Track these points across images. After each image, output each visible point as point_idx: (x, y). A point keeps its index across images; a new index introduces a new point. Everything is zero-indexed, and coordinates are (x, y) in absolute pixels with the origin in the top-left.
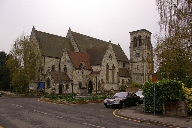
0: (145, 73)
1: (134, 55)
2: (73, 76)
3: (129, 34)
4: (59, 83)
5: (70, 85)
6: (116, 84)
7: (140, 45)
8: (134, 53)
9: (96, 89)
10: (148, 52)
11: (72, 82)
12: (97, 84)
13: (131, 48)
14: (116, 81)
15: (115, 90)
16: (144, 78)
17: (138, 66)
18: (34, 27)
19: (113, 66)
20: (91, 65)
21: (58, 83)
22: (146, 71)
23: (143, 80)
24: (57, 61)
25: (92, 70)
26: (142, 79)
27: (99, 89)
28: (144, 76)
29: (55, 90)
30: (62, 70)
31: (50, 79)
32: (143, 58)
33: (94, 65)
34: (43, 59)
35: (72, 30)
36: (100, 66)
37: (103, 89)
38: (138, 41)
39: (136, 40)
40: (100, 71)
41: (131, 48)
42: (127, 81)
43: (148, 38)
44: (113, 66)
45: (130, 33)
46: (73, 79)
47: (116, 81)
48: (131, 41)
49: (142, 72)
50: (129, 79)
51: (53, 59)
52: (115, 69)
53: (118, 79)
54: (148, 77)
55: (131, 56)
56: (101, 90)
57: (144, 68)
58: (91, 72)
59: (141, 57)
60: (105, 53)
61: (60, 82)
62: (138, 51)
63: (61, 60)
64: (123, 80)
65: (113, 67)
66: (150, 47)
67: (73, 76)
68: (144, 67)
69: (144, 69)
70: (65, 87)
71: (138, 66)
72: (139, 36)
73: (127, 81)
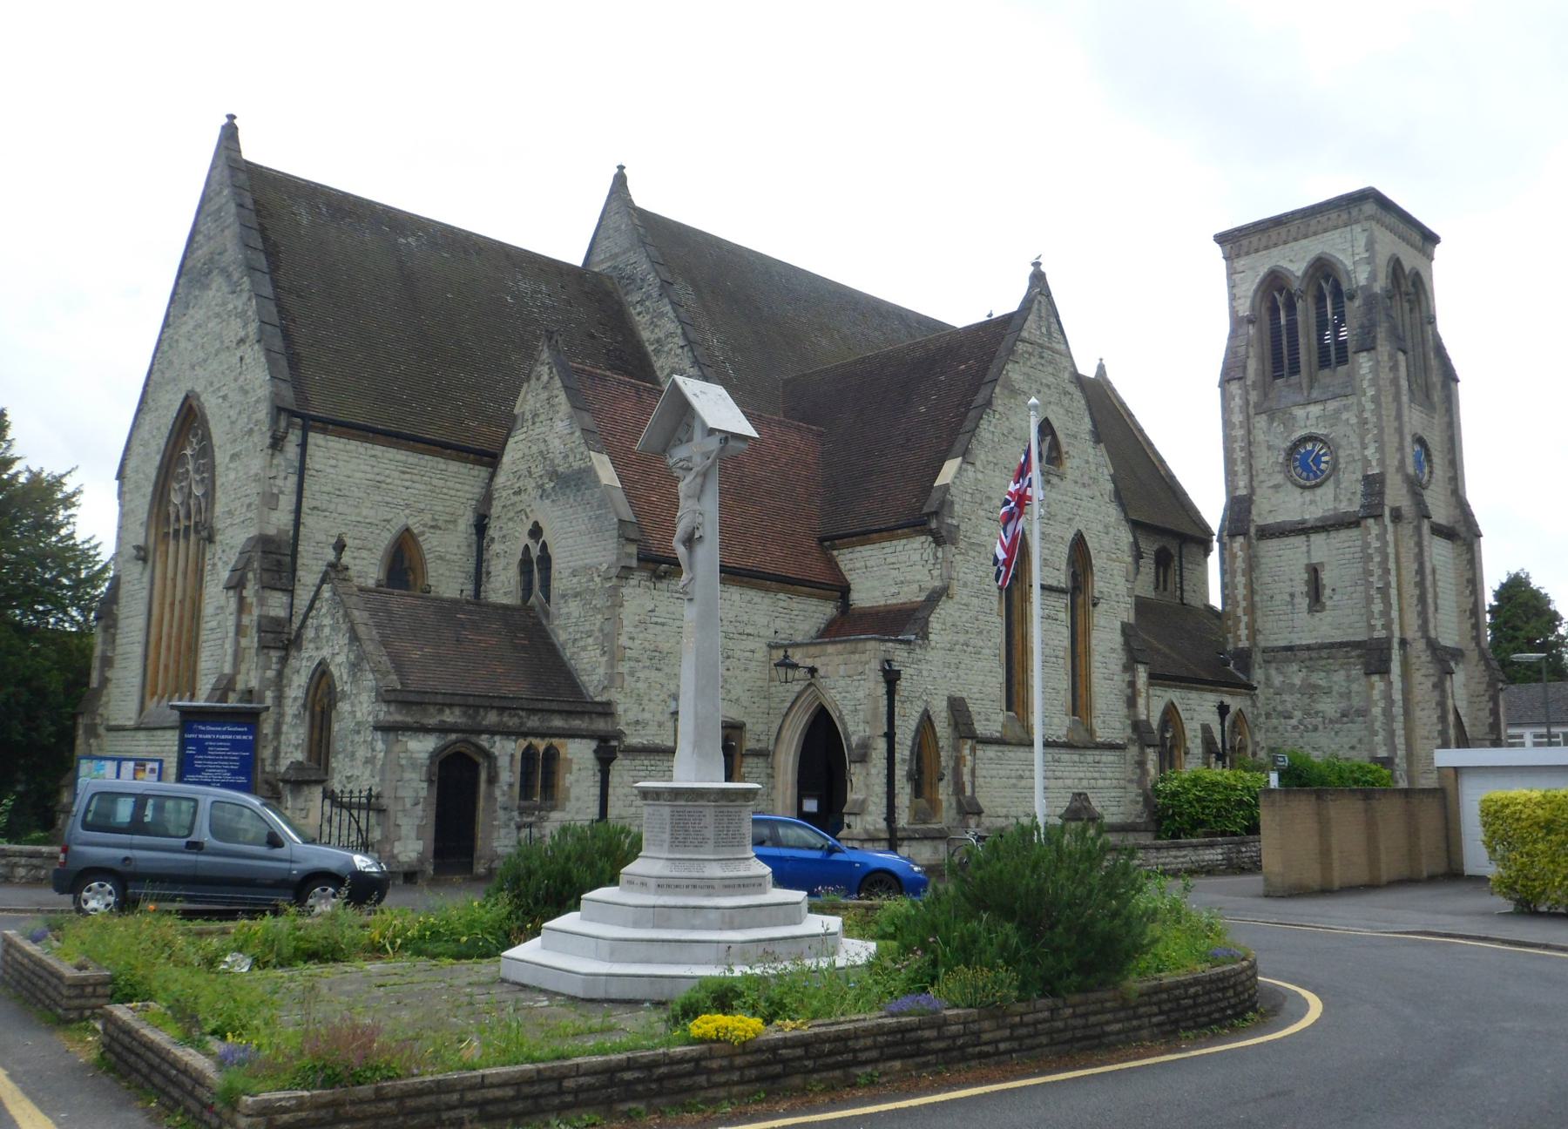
0: (1403, 643)
1: (1269, 460)
2: (614, 655)
3: (1217, 251)
4: (442, 730)
5: (579, 754)
6: (1108, 757)
7: (1334, 356)
8: (1272, 439)
9: (890, 817)
10: (1415, 419)
11: (601, 725)
12: (903, 752)
13: (1235, 388)
14: (1109, 721)
15: (1114, 829)
16: (1397, 696)
17: (1314, 572)
18: (230, 134)
19: (1079, 551)
20: (831, 540)
21: (425, 730)
22: (1413, 620)
23: (1387, 713)
24: (460, 480)
25: (840, 590)
26: (1377, 711)
27: (919, 816)
28: (1395, 667)
29: (381, 811)
30: (503, 586)
31: (339, 671)
32: (1374, 485)
33: (864, 536)
34: (292, 450)
35: (643, 198)
36: (939, 540)
37: (969, 809)
38: (1305, 311)
39: (1291, 307)
40: (936, 597)
41: (1235, 388)
42: (1206, 729)
43: (1406, 286)
44: (1079, 551)
45: (1222, 239)
46: (612, 680)
47: (1109, 721)
48: (1237, 322)
49: (1372, 628)
50: (1235, 703)
51: (413, 458)
52: (1099, 585)
53: (1131, 702)
54: (1439, 686)
55: (1240, 468)
56: (947, 815)
57: (1384, 591)
58: (824, 611)
59: (1351, 480)
60: (989, 403)
61: (451, 717)
62: (1309, 418)
63: (500, 480)
64: (1170, 713)
65: (1072, 561)
66: (1436, 378)
67: (614, 655)
68: (1393, 579)
69: (1393, 592)
70: (508, 775)
71: (1314, 572)
72: (1323, 270)
73: (1206, 729)
